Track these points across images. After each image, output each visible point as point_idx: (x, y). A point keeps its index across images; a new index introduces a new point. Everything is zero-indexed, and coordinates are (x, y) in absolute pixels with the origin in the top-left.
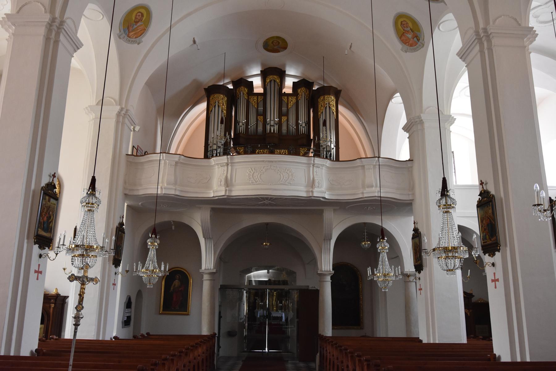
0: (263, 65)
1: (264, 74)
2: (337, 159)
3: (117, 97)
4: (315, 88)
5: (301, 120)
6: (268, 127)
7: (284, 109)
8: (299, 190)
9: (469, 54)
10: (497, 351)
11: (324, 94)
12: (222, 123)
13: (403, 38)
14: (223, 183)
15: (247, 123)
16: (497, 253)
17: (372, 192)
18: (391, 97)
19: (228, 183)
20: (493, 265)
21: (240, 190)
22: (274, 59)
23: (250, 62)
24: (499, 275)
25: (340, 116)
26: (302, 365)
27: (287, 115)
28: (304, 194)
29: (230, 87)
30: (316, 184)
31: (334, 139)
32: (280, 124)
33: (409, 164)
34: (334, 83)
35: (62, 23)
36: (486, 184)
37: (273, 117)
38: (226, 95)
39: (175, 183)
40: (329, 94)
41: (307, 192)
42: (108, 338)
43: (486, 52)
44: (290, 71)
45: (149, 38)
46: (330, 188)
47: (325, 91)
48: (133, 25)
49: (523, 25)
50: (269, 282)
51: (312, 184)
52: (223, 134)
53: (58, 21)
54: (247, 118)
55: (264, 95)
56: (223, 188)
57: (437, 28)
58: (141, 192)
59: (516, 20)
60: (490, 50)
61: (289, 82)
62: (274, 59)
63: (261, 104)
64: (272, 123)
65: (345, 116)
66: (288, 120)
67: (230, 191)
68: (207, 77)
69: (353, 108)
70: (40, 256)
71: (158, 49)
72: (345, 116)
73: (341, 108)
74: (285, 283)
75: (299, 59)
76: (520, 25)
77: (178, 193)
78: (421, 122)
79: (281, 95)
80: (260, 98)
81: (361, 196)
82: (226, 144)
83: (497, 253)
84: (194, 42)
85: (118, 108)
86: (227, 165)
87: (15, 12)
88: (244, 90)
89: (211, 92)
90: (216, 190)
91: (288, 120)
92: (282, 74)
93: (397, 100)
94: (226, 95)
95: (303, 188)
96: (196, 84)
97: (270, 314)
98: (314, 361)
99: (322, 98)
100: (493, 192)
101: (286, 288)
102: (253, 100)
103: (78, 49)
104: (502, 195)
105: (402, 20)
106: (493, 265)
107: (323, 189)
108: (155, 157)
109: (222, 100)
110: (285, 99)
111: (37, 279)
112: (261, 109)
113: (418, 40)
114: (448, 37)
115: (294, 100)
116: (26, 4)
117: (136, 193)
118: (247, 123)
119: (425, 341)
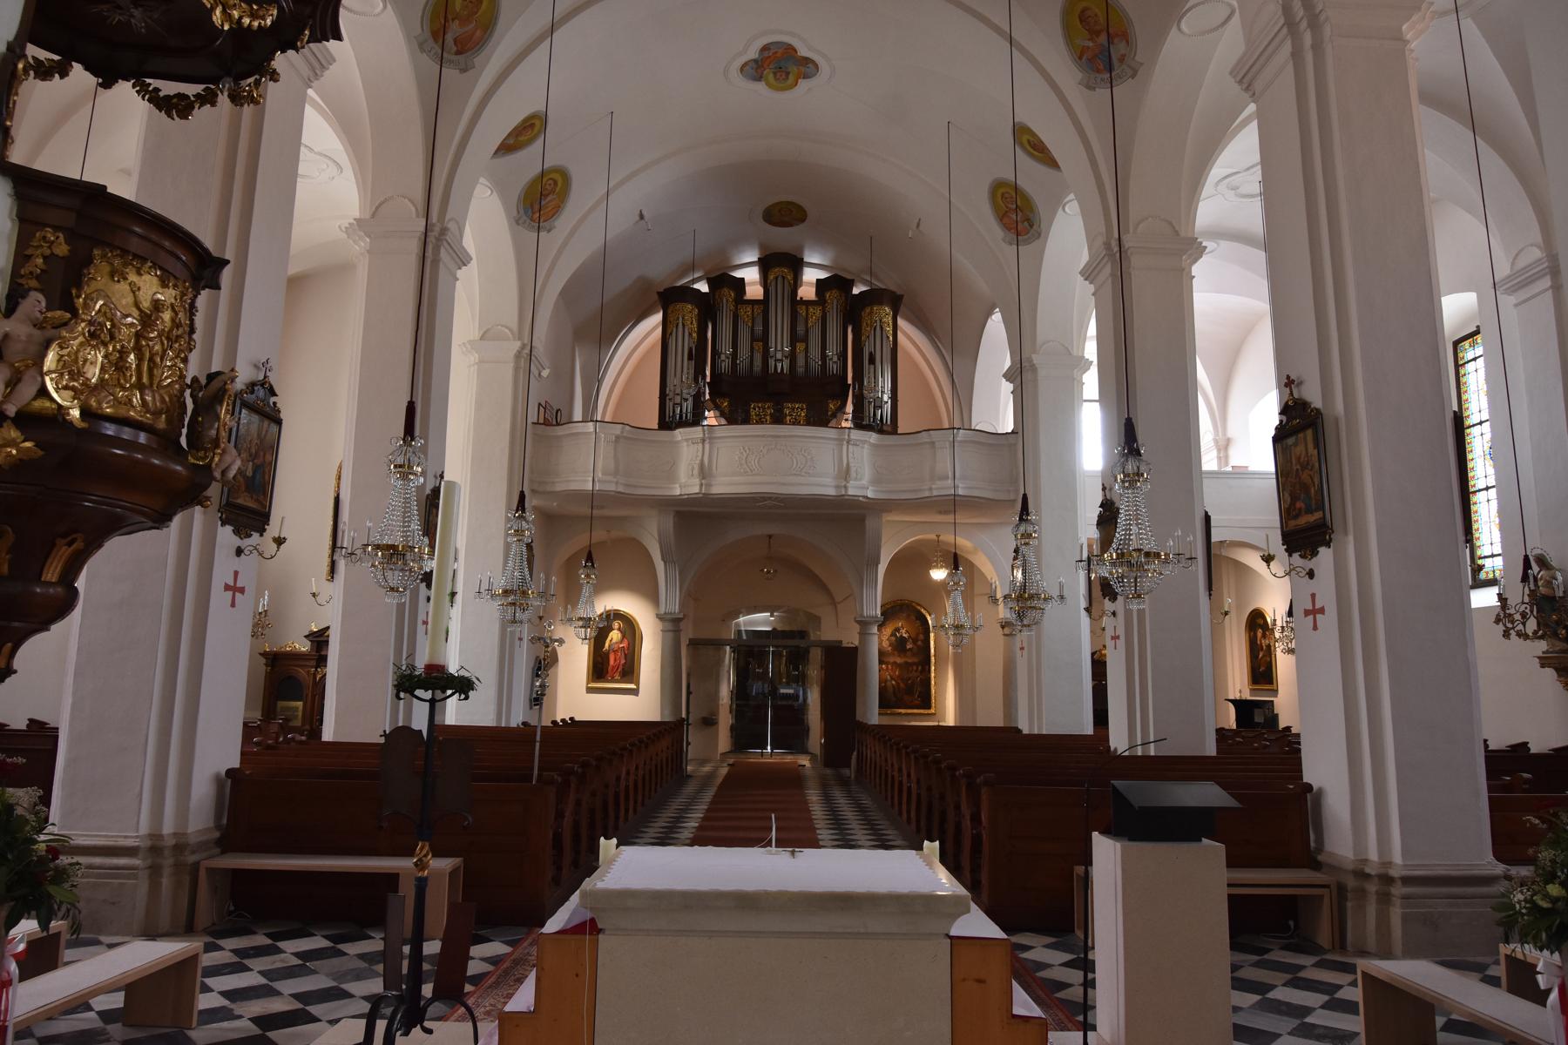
0: (762, 247)
1: (765, 264)
2: (894, 430)
3: (514, 325)
4: (856, 291)
5: (830, 347)
6: (772, 362)
7: (800, 329)
8: (822, 484)
9: (1270, 56)
10: (1113, 744)
11: (872, 304)
12: (690, 358)
13: (1006, 220)
14: (696, 472)
15: (734, 355)
16: (1322, 550)
17: (942, 488)
18: (990, 313)
19: (704, 472)
20: (1114, 614)
21: (726, 484)
22: (783, 238)
23: (739, 242)
24: (1121, 631)
25: (899, 334)
26: (828, 771)
27: (805, 340)
28: (831, 492)
29: (703, 287)
30: (853, 474)
31: (888, 385)
32: (792, 356)
33: (1012, 439)
34: (888, 282)
35: (444, 231)
36: (1300, 383)
37: (780, 344)
38: (697, 307)
39: (616, 473)
40: (881, 303)
41: (837, 487)
42: (513, 724)
43: (1309, 57)
44: (811, 257)
45: (565, 222)
46: (877, 481)
47: (874, 297)
48: (540, 201)
49: (1183, 234)
50: (774, 634)
51: (845, 474)
52: (691, 376)
53: (437, 229)
54: (735, 346)
55: (764, 303)
56: (697, 481)
57: (1174, 28)
58: (559, 488)
59: (1170, 223)
60: (1317, 47)
61: (811, 276)
62: (783, 238)
63: (759, 321)
64: (779, 356)
65: (910, 337)
66: (806, 350)
67: (709, 485)
68: (660, 270)
69: (924, 324)
70: (239, 552)
71: (578, 237)
72: (910, 337)
73: (901, 322)
74: (802, 634)
75: (828, 236)
76: (1177, 233)
77: (621, 489)
78: (1034, 369)
79: (795, 303)
80: (758, 310)
81: (927, 494)
82: (698, 397)
83: (1322, 550)
84: (642, 217)
85: (518, 344)
86: (703, 441)
87: (367, 216)
88: (728, 295)
89: (671, 298)
90: (686, 484)
91: (806, 350)
92: (796, 264)
93: (996, 322)
94: (697, 307)
95: (829, 481)
96: (643, 285)
97: (774, 691)
98: (849, 766)
99: (868, 310)
100: (1316, 400)
101: (802, 644)
102: (746, 312)
103: (323, 68)
104: (1340, 407)
105: (1002, 190)
106: (1114, 614)
107: (864, 482)
108: (581, 428)
109: (689, 312)
110: (802, 310)
111: (233, 605)
112: (759, 328)
113: (1031, 226)
114: (1069, 237)
115: (818, 313)
116: (386, 200)
117: (549, 488)
118: (734, 355)
119: (1026, 731)
